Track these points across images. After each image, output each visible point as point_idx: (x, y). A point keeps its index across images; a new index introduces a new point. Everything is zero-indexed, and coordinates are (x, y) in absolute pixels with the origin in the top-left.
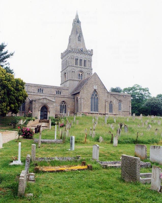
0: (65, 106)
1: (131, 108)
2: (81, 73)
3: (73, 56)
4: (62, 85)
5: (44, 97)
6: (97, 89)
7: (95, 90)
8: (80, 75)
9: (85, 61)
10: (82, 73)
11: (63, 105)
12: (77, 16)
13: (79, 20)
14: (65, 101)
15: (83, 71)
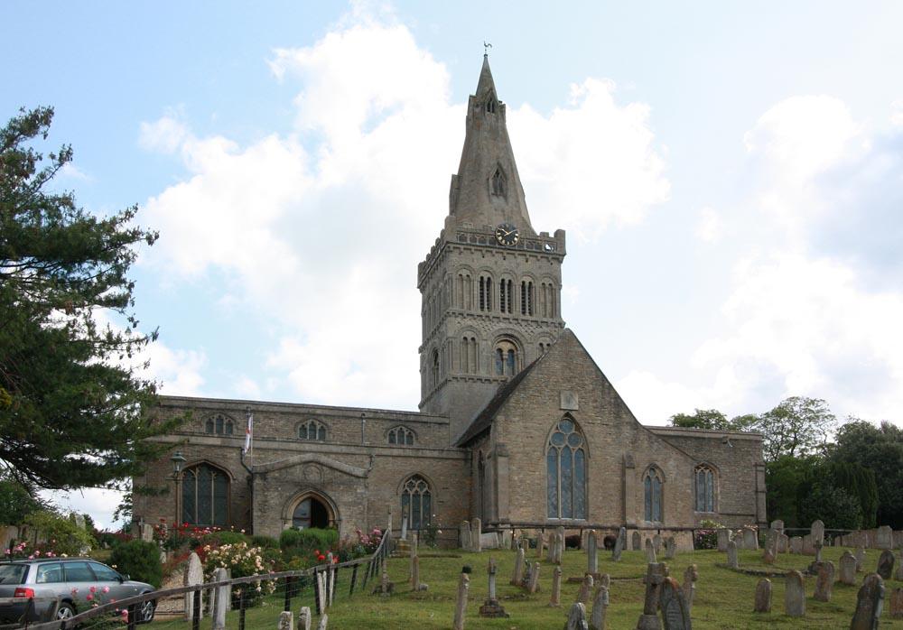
0: (427, 495)
1: (763, 497)
2: (506, 347)
3: (466, 267)
4: (425, 406)
5: (308, 457)
6: (577, 408)
7: (567, 415)
8: (505, 353)
9: (527, 289)
10: (513, 348)
11: (416, 495)
12: (486, 78)
13: (499, 99)
14: (427, 473)
15: (516, 334)
